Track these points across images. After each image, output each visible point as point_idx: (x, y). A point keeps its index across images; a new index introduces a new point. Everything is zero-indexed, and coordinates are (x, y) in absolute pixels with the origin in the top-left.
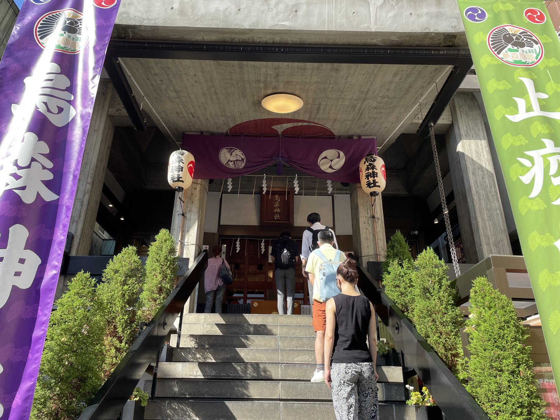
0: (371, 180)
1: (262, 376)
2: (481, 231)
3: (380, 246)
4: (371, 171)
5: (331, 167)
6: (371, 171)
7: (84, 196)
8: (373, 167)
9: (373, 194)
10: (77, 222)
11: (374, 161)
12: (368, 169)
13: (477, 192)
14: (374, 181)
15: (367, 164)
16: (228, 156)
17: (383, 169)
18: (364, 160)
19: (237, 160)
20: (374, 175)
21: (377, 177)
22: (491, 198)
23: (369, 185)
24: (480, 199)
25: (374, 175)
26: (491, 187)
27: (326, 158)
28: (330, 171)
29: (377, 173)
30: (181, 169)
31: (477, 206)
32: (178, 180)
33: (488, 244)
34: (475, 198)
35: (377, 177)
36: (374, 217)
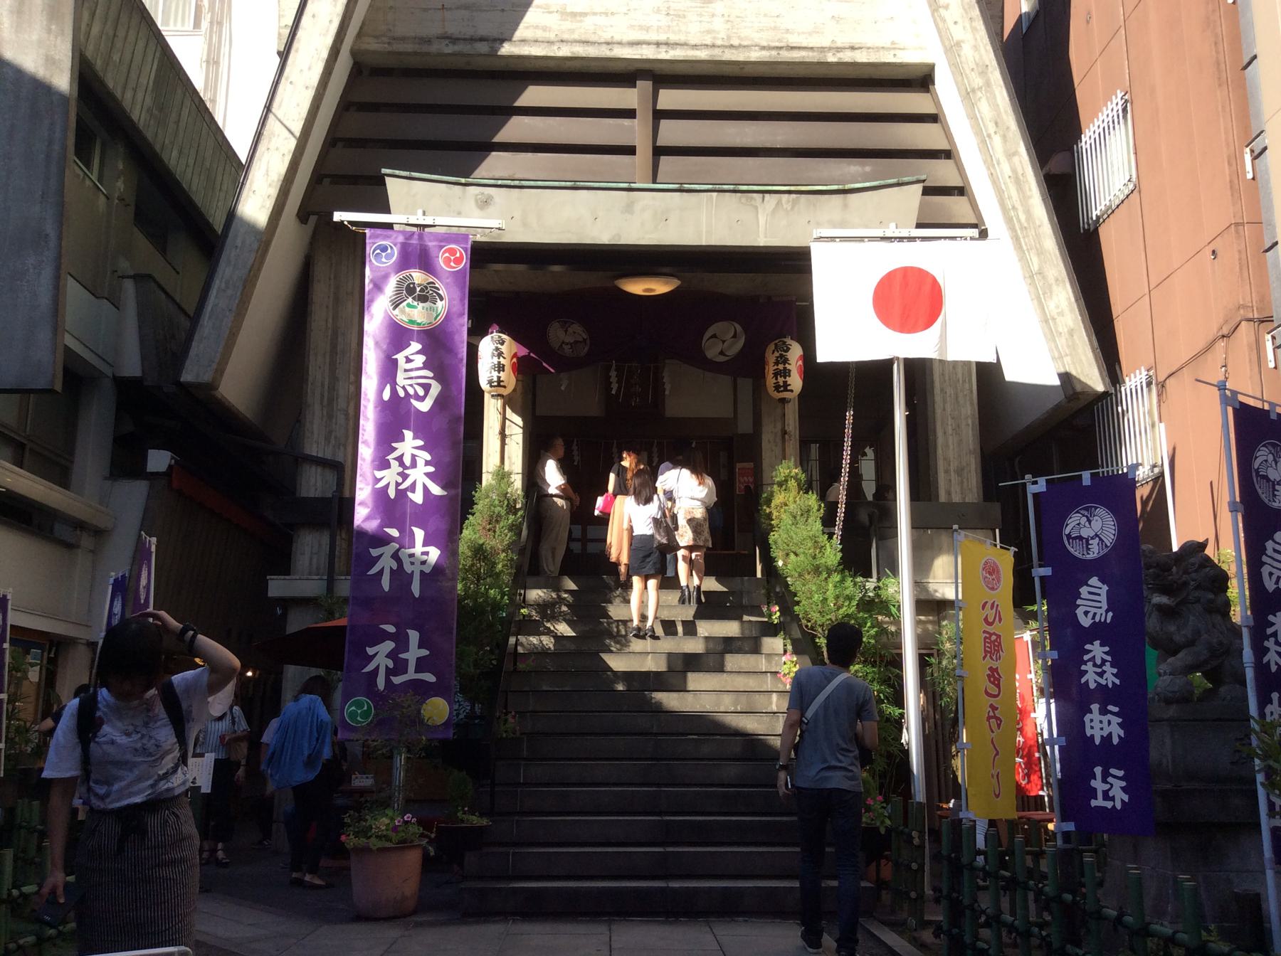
0: (781, 380)
1: (773, 468)
2: (940, 451)
3: (1115, 163)
4: (781, 367)
5: (722, 353)
6: (781, 367)
7: (348, 403)
8: (786, 361)
9: (783, 401)
10: (345, 446)
11: (788, 349)
12: (777, 363)
13: (942, 390)
14: (785, 382)
15: (777, 354)
16: (561, 334)
17: (800, 363)
18: (772, 346)
19: (576, 342)
20: (786, 373)
22: (961, 400)
23: (777, 387)
24: (945, 402)
26: (964, 381)
27: (714, 336)
28: (722, 359)
30: (500, 368)
31: (939, 411)
32: (499, 385)
33: (947, 472)
34: (938, 398)
36: (996, 124)
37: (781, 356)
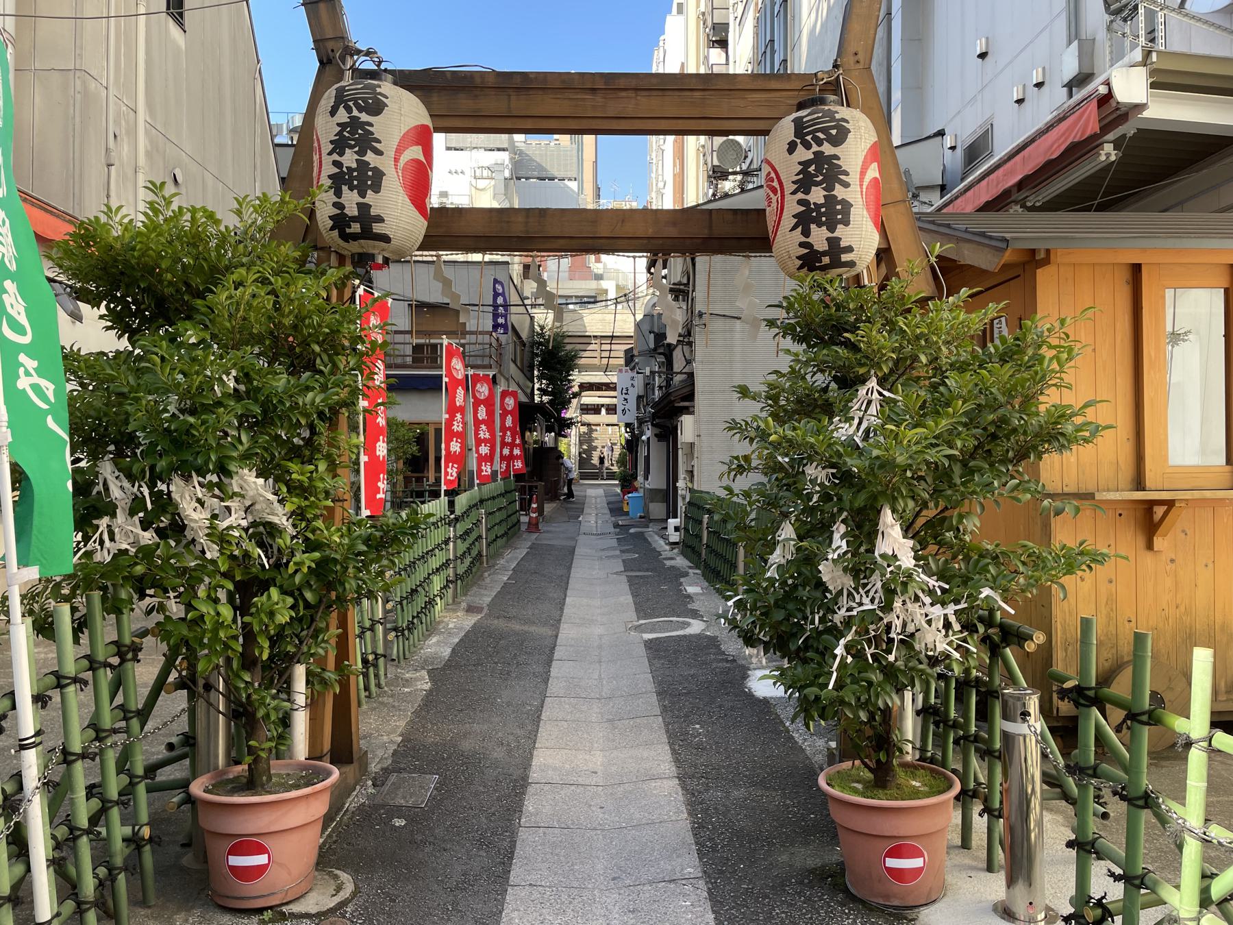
0: (819, 237)
4: (817, 195)
12: (804, 184)
14: (834, 243)
15: (342, 116)
21: (847, 223)
25: (362, 178)
29: (379, 175)
35: (847, 223)
37: (354, 123)
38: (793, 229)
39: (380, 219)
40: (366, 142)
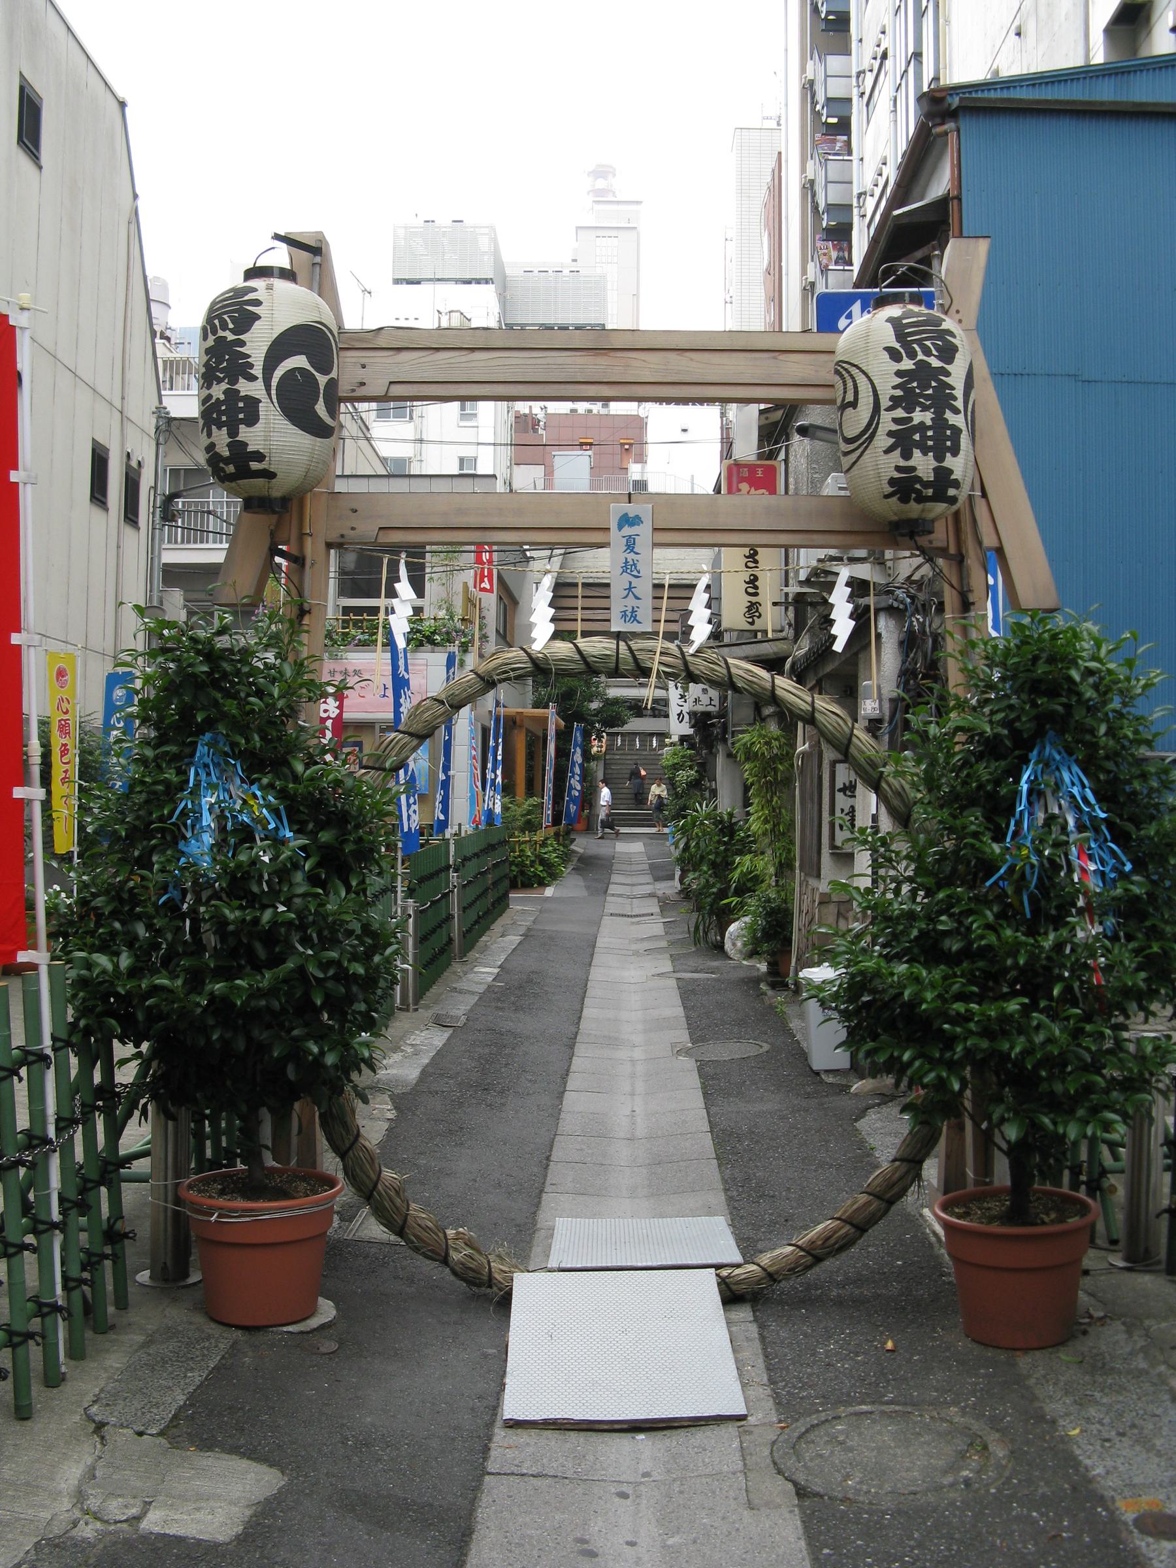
12: (906, 400)
38: (888, 451)
39: (259, 456)
40: (239, 368)
